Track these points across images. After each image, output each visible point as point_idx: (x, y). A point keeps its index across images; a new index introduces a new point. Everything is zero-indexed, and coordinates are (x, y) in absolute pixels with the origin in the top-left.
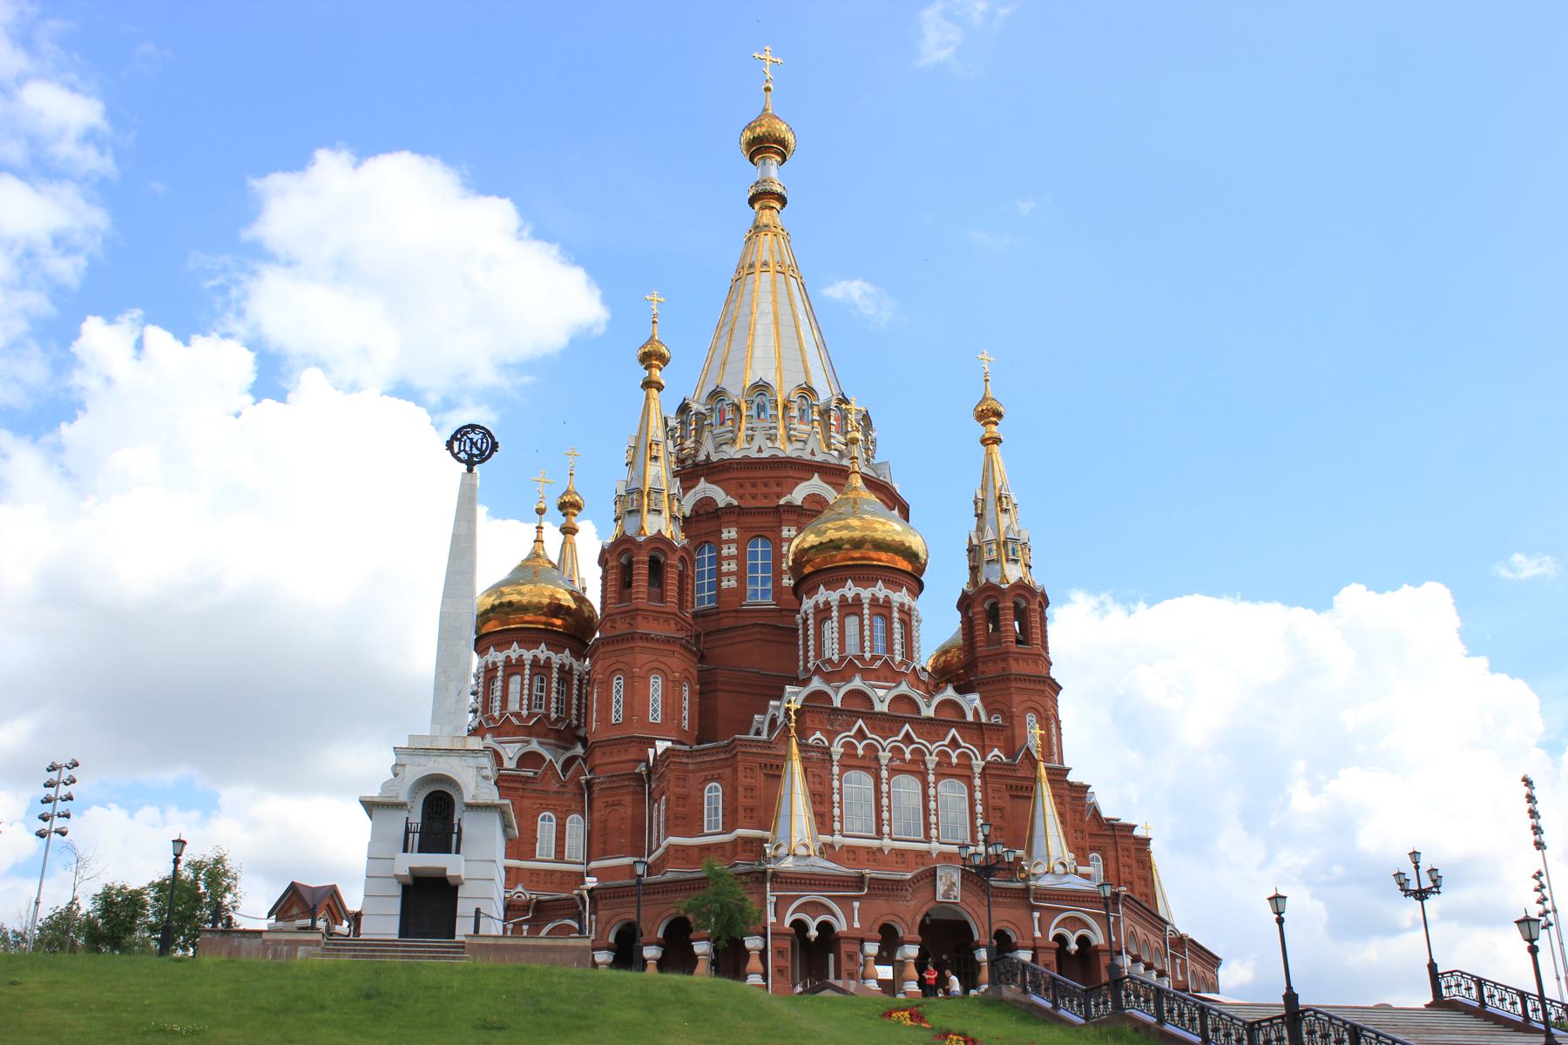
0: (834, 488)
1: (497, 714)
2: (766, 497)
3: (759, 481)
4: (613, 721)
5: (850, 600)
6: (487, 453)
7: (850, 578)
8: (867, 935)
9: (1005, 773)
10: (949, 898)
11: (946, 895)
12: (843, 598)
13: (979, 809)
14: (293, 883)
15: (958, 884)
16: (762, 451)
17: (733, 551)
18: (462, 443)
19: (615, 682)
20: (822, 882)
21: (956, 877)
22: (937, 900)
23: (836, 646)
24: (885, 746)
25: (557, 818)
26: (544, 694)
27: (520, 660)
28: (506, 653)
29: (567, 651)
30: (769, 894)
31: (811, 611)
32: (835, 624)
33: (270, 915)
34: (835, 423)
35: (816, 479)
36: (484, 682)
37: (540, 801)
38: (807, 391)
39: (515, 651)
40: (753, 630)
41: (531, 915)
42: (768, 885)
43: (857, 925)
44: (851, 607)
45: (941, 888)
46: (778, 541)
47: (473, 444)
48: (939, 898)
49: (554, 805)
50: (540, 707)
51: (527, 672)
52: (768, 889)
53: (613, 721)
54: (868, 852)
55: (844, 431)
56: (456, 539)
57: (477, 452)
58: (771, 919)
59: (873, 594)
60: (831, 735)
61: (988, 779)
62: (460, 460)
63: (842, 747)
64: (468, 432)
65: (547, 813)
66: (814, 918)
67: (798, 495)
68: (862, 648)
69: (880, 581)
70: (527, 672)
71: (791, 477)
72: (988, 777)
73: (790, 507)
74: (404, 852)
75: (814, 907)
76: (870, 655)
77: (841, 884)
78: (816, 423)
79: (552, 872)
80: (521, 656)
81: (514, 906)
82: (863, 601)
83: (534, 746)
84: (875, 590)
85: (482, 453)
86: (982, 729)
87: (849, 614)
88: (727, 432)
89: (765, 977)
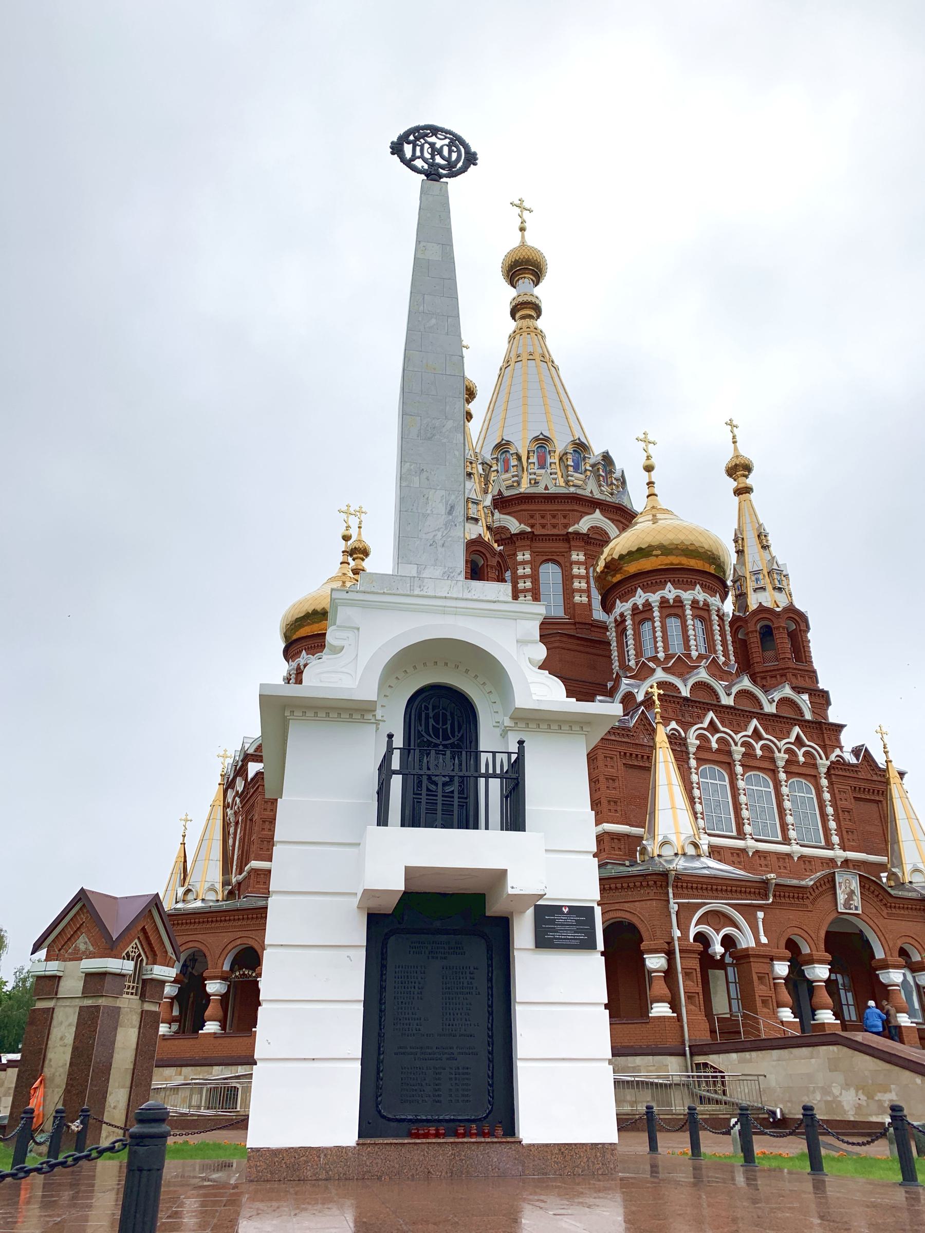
0: (613, 522)
1: (632, 663)
2: (554, 527)
3: (548, 513)
6: (460, 165)
7: (670, 581)
8: (774, 952)
9: (847, 774)
10: (850, 909)
11: (847, 905)
13: (830, 810)
14: (82, 890)
15: (858, 892)
16: (548, 490)
17: (528, 570)
18: (418, 148)
20: (700, 886)
21: (855, 885)
22: (840, 910)
24: (737, 740)
29: (698, 587)
30: (672, 901)
31: (628, 614)
33: (36, 948)
34: (603, 474)
40: (553, 639)
42: (670, 891)
43: (764, 940)
44: (673, 609)
45: (841, 898)
46: (567, 564)
47: (435, 151)
48: (841, 909)
51: (656, 614)
52: (671, 895)
54: (732, 854)
55: (609, 483)
56: (421, 266)
57: (443, 162)
58: (677, 933)
60: (686, 726)
61: (834, 779)
62: (415, 169)
63: (696, 739)
64: (427, 135)
67: (584, 525)
68: (687, 646)
69: (698, 586)
70: (656, 614)
71: (577, 511)
72: (833, 776)
73: (577, 534)
74: (379, 825)
75: (717, 918)
77: (743, 889)
80: (647, 600)
85: (451, 165)
86: (821, 729)
88: (513, 476)
89: (675, 1007)
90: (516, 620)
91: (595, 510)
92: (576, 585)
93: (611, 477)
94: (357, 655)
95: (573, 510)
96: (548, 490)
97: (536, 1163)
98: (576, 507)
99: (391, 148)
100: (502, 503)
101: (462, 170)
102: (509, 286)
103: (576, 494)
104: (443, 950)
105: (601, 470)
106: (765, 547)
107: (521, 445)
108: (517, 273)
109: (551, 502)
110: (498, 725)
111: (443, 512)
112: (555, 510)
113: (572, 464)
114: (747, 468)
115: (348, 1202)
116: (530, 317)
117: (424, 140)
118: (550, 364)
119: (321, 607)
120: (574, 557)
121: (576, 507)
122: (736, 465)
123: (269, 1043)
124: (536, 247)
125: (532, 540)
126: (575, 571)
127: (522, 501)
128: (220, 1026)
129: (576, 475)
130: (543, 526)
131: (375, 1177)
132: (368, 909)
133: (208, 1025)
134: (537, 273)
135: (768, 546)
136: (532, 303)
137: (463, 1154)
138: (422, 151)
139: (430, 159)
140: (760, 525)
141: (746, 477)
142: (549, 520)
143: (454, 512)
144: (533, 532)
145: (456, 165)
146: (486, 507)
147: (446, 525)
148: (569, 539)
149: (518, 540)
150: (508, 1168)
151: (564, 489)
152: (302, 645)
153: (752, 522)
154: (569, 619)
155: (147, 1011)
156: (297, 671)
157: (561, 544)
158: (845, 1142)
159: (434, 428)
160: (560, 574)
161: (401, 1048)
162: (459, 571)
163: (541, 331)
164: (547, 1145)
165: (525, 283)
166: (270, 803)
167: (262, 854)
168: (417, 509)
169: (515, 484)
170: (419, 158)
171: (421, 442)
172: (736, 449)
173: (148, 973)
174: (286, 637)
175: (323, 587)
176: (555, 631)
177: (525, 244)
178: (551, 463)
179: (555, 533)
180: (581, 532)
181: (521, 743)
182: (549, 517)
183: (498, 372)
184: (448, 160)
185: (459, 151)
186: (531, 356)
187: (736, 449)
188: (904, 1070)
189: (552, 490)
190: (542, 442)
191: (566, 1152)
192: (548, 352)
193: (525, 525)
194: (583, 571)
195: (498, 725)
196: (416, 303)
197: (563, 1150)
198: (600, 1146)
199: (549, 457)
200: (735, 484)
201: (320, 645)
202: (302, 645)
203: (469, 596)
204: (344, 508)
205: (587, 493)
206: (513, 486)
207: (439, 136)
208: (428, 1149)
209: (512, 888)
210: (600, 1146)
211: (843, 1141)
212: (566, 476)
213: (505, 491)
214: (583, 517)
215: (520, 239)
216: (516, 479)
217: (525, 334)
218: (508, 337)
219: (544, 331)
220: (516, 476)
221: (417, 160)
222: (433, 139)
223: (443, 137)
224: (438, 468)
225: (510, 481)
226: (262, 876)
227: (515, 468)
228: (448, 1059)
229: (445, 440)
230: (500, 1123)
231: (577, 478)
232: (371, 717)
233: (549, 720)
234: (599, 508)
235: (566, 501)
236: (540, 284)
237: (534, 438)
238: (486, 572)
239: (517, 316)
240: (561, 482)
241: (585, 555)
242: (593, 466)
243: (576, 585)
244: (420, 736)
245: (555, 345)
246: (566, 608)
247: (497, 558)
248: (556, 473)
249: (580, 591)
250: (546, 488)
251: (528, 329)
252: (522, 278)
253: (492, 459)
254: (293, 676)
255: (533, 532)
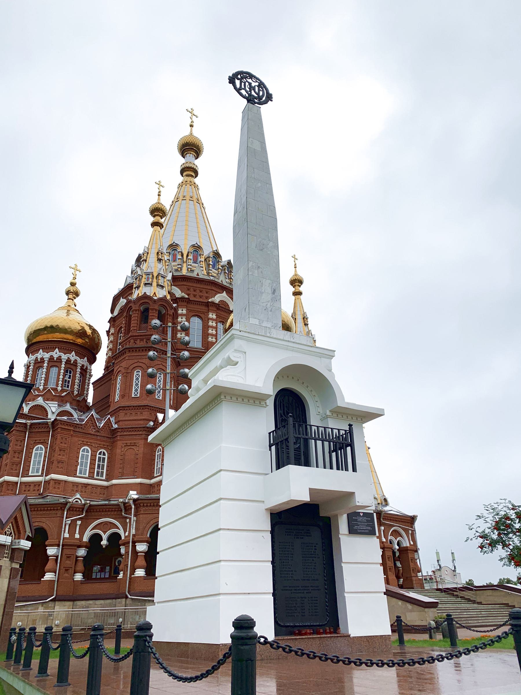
1: (41, 388)
2: (201, 297)
3: (198, 289)
4: (133, 396)
5: (55, 359)
6: (264, 99)
12: (51, 358)
16: (199, 276)
18: (243, 84)
19: (135, 373)
23: (43, 381)
25: (91, 450)
26: (70, 380)
27: (59, 359)
28: (51, 353)
29: (86, 358)
32: (45, 370)
34: (227, 272)
35: (224, 294)
36: (33, 369)
37: (82, 440)
38: (217, 255)
39: (56, 354)
41: (84, 515)
44: (54, 363)
46: (206, 319)
47: (251, 88)
49: (91, 443)
50: (68, 387)
53: (133, 396)
59: (68, 358)
62: (241, 94)
65: (86, 447)
66: (105, 532)
67: (217, 299)
68: (57, 385)
73: (213, 303)
76: (61, 388)
78: (220, 270)
79: (86, 485)
81: (73, 508)
82: (63, 360)
83: (68, 407)
84: (70, 356)
85: (260, 98)
87: (52, 366)
88: (178, 265)
90: (321, 357)
91: (223, 292)
92: (210, 331)
93: (231, 274)
94: (245, 367)
95: (212, 290)
96: (199, 276)
97: (357, 646)
98: (213, 288)
99: (229, 79)
100: (177, 280)
101: (265, 102)
102: (182, 157)
103: (214, 281)
104: (301, 534)
105: (226, 270)
106: (306, 325)
107: (185, 248)
108: (187, 150)
109: (200, 283)
110: (319, 413)
111: (270, 292)
112: (202, 288)
113: (212, 264)
114: (301, 282)
115: (273, 672)
116: (192, 176)
117: (246, 80)
118: (201, 205)
119: (56, 324)
120: (210, 316)
121: (213, 288)
122: (296, 279)
123: (227, 585)
124: (199, 138)
125: (188, 303)
126: (210, 323)
127: (184, 280)
128: (83, 576)
129: (213, 270)
130: (195, 296)
131: (284, 657)
132: (271, 510)
133: (47, 575)
134: (198, 152)
135: (308, 324)
136: (192, 168)
137: (324, 643)
138: (245, 85)
139: (249, 91)
140: (304, 313)
141: (300, 286)
142: (198, 293)
143: (276, 293)
144: (189, 298)
145: (262, 98)
146: (168, 280)
147: (272, 299)
148: (209, 305)
149: (180, 301)
150: (345, 650)
151: (207, 277)
152: (40, 346)
153: (300, 311)
154: (204, 350)
155: (14, 568)
156: (35, 361)
157: (203, 307)
158: (475, 631)
159: (264, 244)
160: (202, 324)
161: (285, 587)
162: (280, 326)
163: (197, 186)
164: (361, 637)
165: (190, 157)
166: (20, 441)
167: (13, 472)
168: (257, 288)
169: (179, 269)
170: (243, 89)
171: (257, 251)
172: (296, 271)
173: (16, 544)
174: (29, 340)
175: (54, 312)
176: (198, 356)
177: (190, 134)
178: (200, 261)
179: (201, 301)
180: (215, 302)
181: (350, 425)
182: (198, 291)
183: (171, 203)
184: (258, 94)
185: (263, 91)
186: (191, 199)
187: (296, 271)
188: (393, 598)
189: (201, 276)
190: (197, 249)
191: (370, 640)
192: (200, 198)
193: (184, 293)
194: (214, 324)
195: (319, 413)
196: (250, 172)
197: (368, 639)
198: (384, 636)
199: (199, 257)
200: (294, 289)
201: (52, 347)
202: (40, 346)
203: (292, 340)
204: (73, 266)
205: (220, 281)
206: (178, 270)
207: (253, 79)
208: (308, 641)
209: (358, 502)
210: (384, 636)
211: (473, 630)
212: (208, 269)
213: (174, 272)
214: (217, 294)
215: (189, 131)
216: (180, 266)
217: (188, 185)
218: (178, 184)
219: (199, 186)
220: (180, 265)
221: (243, 90)
222: (250, 80)
223: (255, 81)
224: (266, 267)
225: (177, 267)
226: (11, 486)
227: (180, 260)
228: (307, 593)
229: (269, 252)
230: (333, 626)
231: (214, 272)
232: (264, 404)
233: (357, 415)
234: (225, 291)
235: (207, 284)
236: (198, 159)
237: (192, 245)
238: (166, 318)
239: (184, 174)
240: (205, 272)
241: (216, 315)
242: (222, 266)
243: (210, 331)
244: (281, 416)
245: (204, 195)
246: (203, 343)
247: (173, 311)
248: (203, 267)
249: (212, 335)
250: (198, 275)
251: (190, 183)
252: (189, 153)
253: (167, 252)
254: (32, 364)
255: (189, 298)
